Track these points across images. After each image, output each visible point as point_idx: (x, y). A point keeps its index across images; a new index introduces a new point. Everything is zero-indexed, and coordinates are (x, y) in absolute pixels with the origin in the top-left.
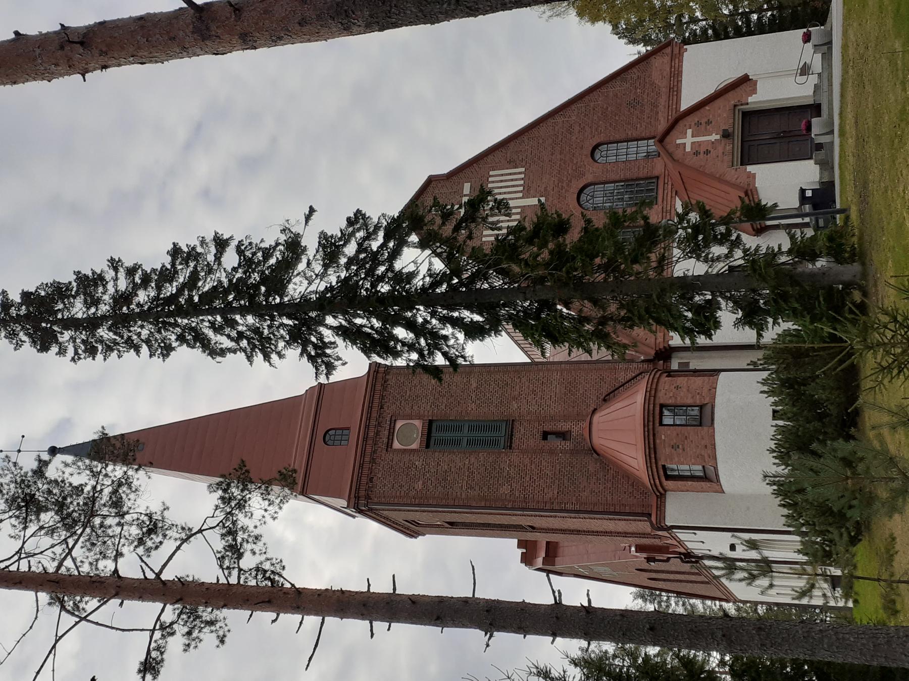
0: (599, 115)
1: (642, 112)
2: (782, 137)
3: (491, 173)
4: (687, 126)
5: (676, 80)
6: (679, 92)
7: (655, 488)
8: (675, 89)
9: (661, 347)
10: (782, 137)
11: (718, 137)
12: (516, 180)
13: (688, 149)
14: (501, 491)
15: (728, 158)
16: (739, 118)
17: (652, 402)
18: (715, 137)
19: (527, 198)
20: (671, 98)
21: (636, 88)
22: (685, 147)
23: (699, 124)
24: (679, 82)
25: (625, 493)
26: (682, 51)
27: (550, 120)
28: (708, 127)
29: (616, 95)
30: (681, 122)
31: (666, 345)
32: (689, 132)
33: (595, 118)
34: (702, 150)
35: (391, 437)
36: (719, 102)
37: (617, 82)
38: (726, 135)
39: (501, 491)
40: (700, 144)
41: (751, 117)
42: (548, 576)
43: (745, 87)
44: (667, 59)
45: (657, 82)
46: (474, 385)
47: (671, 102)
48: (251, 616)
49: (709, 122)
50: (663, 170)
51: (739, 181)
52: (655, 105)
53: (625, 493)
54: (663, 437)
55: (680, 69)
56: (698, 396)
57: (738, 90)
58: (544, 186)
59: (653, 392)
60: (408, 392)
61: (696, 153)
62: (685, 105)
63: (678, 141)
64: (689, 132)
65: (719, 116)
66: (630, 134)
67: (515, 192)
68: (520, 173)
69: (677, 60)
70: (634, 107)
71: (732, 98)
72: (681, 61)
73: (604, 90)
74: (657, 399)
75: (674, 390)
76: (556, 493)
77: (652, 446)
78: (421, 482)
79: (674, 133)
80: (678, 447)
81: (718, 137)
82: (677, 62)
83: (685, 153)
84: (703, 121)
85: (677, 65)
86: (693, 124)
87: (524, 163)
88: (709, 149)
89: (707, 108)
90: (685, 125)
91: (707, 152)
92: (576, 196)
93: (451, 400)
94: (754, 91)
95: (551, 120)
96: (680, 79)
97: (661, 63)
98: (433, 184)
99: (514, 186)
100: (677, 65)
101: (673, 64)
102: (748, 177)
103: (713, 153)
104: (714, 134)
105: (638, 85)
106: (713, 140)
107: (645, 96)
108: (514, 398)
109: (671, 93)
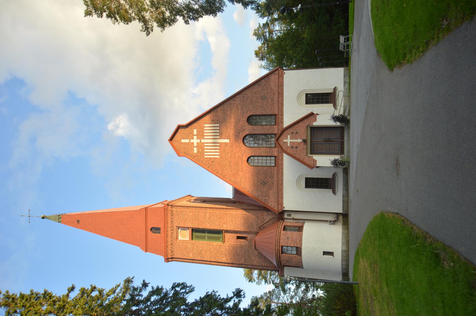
0: (249, 101)
1: (268, 102)
2: (327, 141)
4: (288, 134)
5: (281, 88)
6: (286, 154)
7: (279, 264)
8: (281, 93)
9: (281, 211)
10: (327, 141)
11: (301, 141)
13: (289, 145)
15: (305, 151)
16: (309, 130)
17: (278, 246)
18: (299, 141)
20: (279, 98)
21: (264, 90)
22: (287, 144)
23: (292, 133)
24: (283, 89)
25: (269, 263)
26: (283, 74)
27: (228, 102)
28: (297, 135)
29: (256, 93)
30: (285, 131)
31: (282, 210)
32: (289, 136)
33: (248, 103)
34: (295, 146)
35: (177, 235)
36: (301, 124)
37: (256, 86)
38: (305, 141)
40: (293, 143)
41: (314, 129)
43: (312, 118)
44: (277, 77)
45: (273, 88)
47: (279, 99)
49: (297, 133)
50: (278, 132)
51: (310, 163)
52: (273, 100)
53: (269, 263)
54: (283, 258)
55: (283, 83)
56: (295, 243)
57: (309, 119)
58: (228, 134)
59: (279, 241)
60: (182, 217)
61: (292, 147)
62: (286, 124)
63: (285, 141)
64: (289, 136)
65: (301, 130)
66: (263, 113)
69: (281, 78)
70: (264, 99)
71: (306, 122)
72: (283, 79)
73: (250, 89)
74: (280, 243)
76: (243, 261)
77: (279, 261)
79: (283, 136)
80: (289, 261)
81: (301, 141)
82: (281, 79)
83: (287, 147)
84: (295, 132)
85: (281, 81)
86: (290, 133)
87: (219, 122)
88: (297, 146)
90: (287, 133)
91: (297, 147)
92: (242, 140)
93: (199, 222)
94: (315, 120)
95: (228, 102)
96: (282, 88)
97: (274, 78)
100: (281, 81)
101: (279, 80)
102: (314, 162)
103: (299, 149)
104: (299, 139)
105: (265, 88)
106: (299, 142)
108: (225, 223)
109: (279, 95)
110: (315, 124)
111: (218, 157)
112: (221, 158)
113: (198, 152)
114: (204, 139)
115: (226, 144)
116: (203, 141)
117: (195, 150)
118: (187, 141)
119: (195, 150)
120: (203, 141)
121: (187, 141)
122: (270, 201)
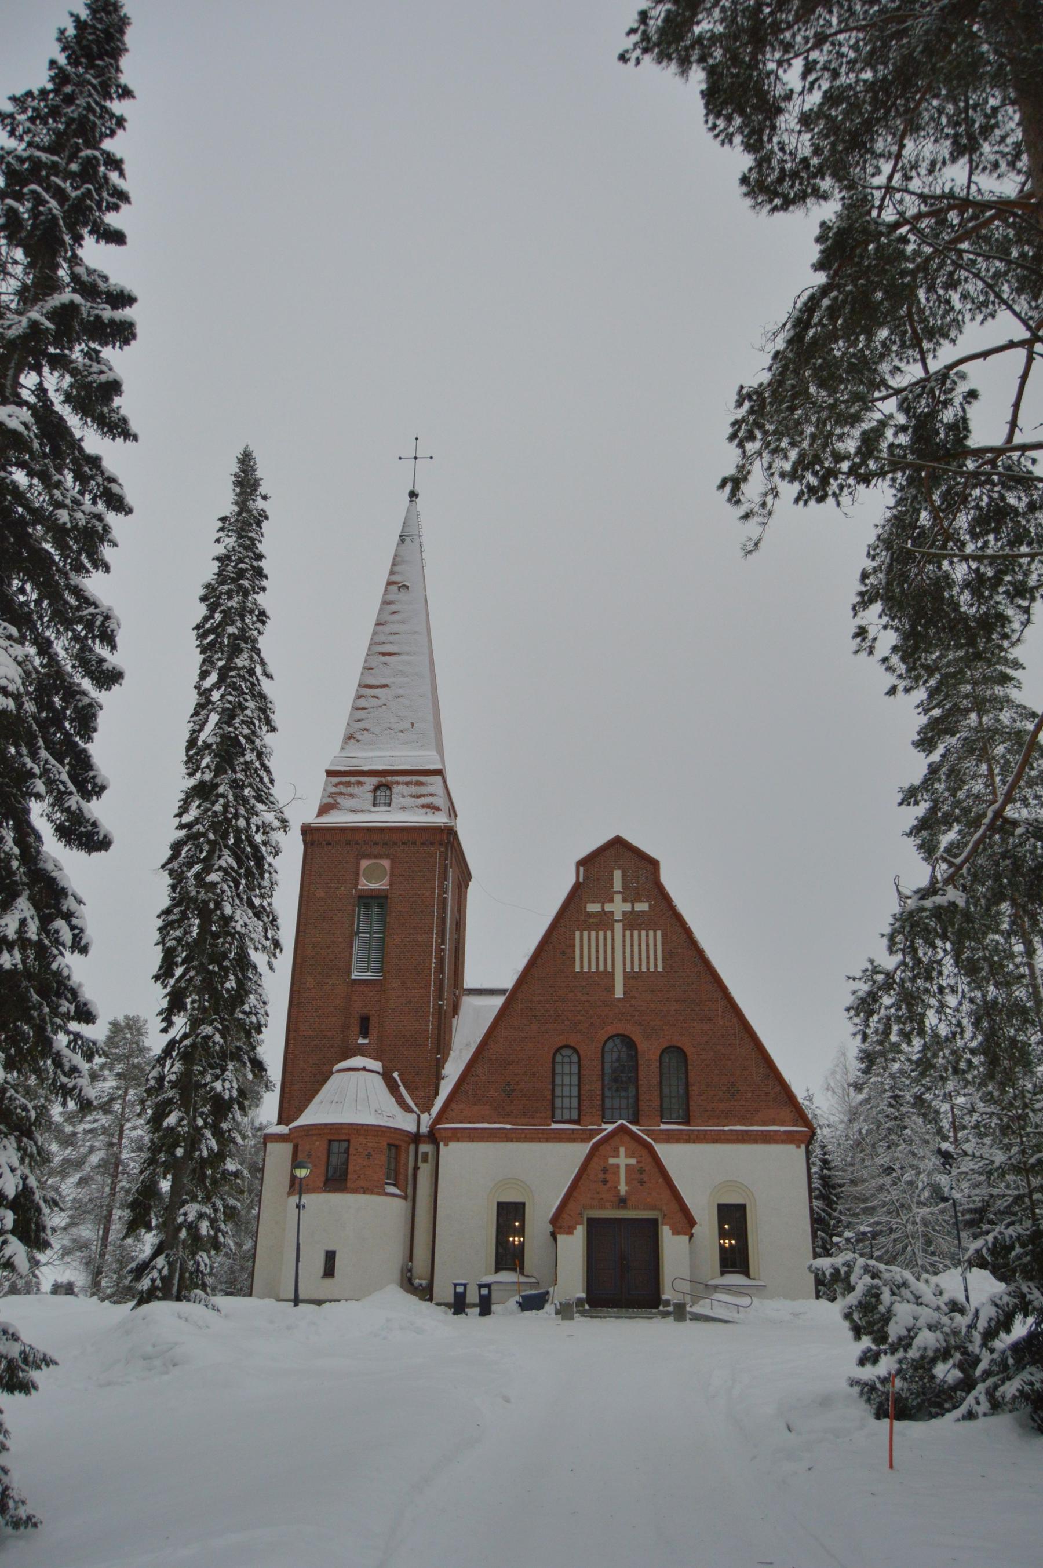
3: (659, 933)
12: (648, 963)
13: (612, 1161)
14: (309, 978)
18: (623, 1188)
19: (624, 977)
23: (641, 1171)
34: (608, 1177)
39: (309, 978)
41: (651, 1229)
42: (503, 992)
46: (420, 939)
48: (1013, 424)
49: (642, 1183)
61: (605, 1170)
67: (632, 963)
68: (656, 966)
75: (366, 1153)
78: (323, 894)
84: (645, 1178)
89: (661, 1180)
91: (605, 1182)
94: (676, 1232)
98: (650, 867)
99: (640, 960)
102: (569, 1227)
107: (742, 1103)
110: (666, 1231)
111: (578, 970)
112: (576, 975)
113: (590, 915)
114: (624, 930)
115: (611, 989)
116: (618, 927)
117: (593, 907)
118: (618, 885)
119: (593, 907)
120: (618, 927)
121: (618, 885)
122: (462, 1106)
